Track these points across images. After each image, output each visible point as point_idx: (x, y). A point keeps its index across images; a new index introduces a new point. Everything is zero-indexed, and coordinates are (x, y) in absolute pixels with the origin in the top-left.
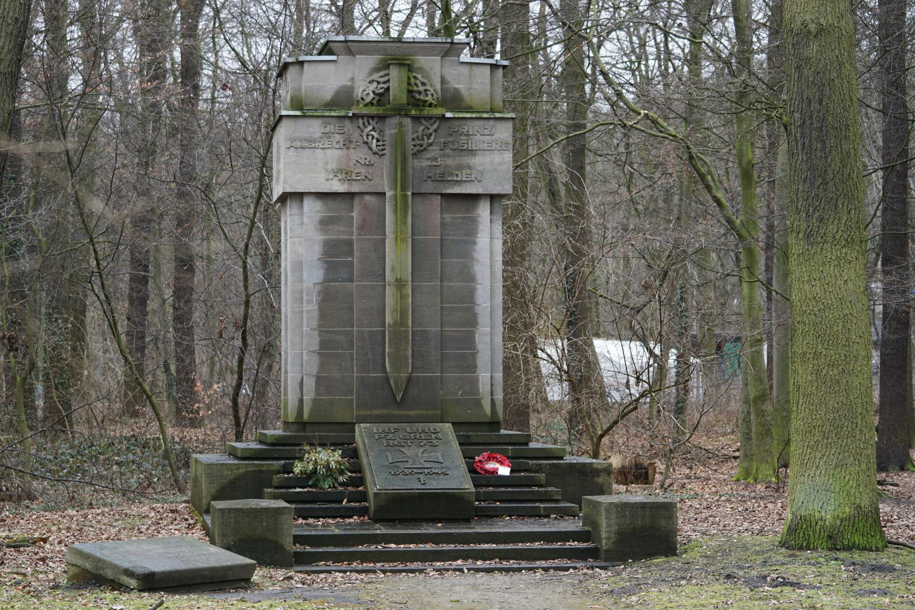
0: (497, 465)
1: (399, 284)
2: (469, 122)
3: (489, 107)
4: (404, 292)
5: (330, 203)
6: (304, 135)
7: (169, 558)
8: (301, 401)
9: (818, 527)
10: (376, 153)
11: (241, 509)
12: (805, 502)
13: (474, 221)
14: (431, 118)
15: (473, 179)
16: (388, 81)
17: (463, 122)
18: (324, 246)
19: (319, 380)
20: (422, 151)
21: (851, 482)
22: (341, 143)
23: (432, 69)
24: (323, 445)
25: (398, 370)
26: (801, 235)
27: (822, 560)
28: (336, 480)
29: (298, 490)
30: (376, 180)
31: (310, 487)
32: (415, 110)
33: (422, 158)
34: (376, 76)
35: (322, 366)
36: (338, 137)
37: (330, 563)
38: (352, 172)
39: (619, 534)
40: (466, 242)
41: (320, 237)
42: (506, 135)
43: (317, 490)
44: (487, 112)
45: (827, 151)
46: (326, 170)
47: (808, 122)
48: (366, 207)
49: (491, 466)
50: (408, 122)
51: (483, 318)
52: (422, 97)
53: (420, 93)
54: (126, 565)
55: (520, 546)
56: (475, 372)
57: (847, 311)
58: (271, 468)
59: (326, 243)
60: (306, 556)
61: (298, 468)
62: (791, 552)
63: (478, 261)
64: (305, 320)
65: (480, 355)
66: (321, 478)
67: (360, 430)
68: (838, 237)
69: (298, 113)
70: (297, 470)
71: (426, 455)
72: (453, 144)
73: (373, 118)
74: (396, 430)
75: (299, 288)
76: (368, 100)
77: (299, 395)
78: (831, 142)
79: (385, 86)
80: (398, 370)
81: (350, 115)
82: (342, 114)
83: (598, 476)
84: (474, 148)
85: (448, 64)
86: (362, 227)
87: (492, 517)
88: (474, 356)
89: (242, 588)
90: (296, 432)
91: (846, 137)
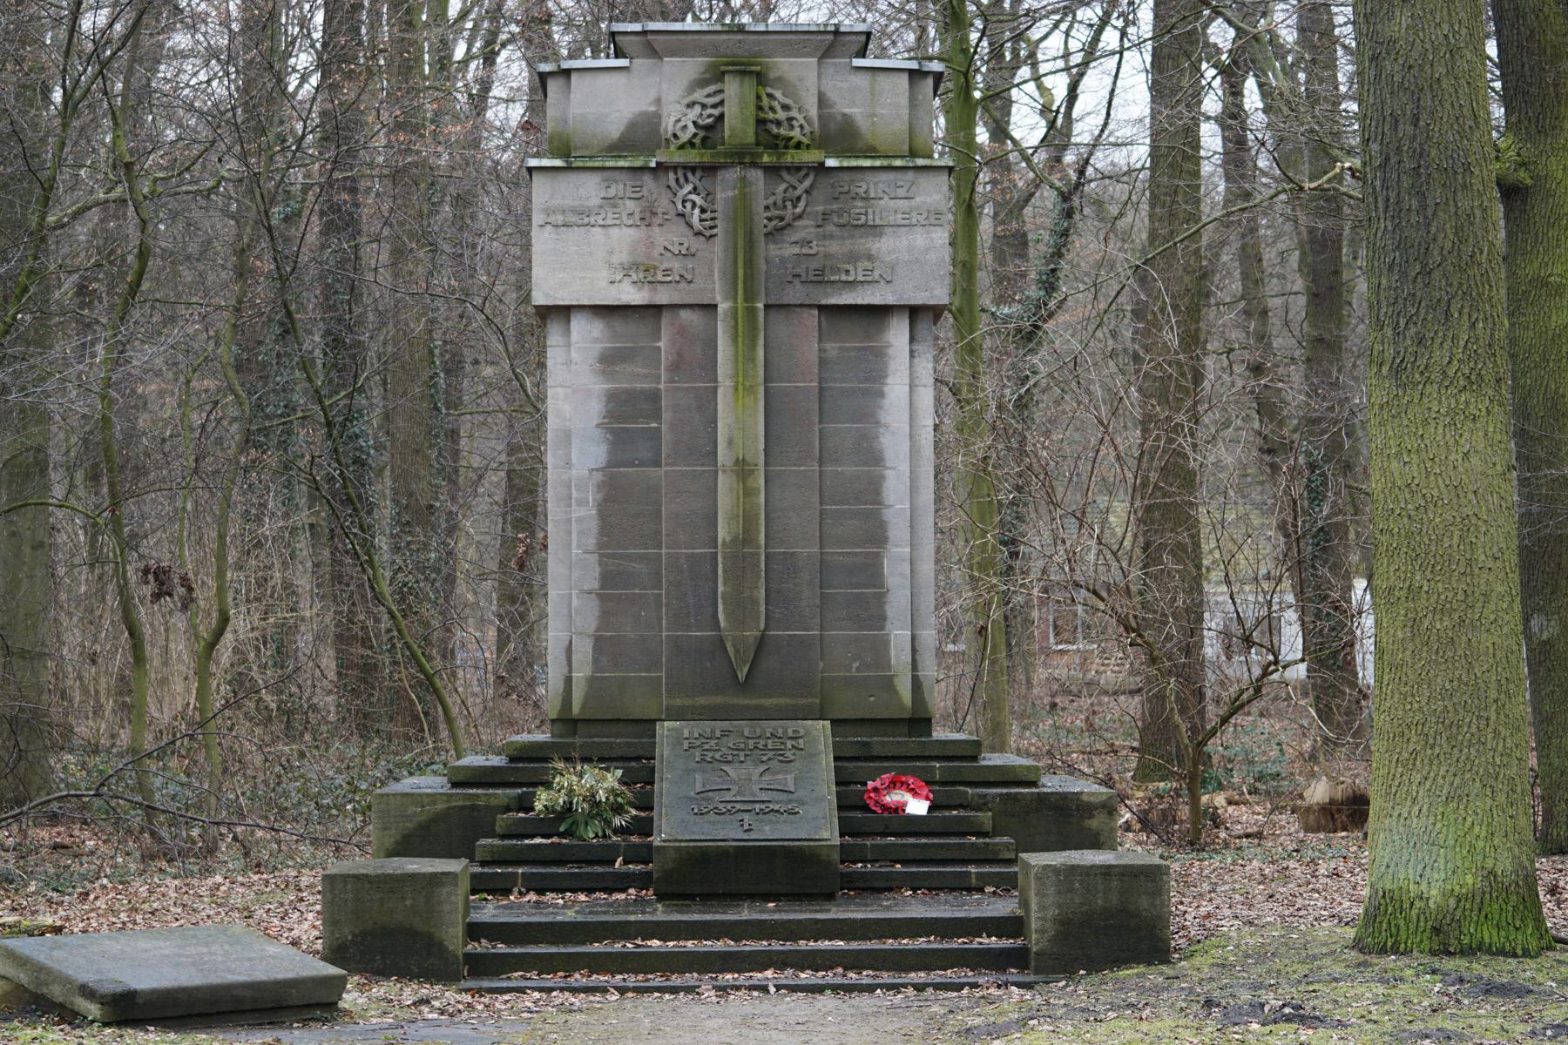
0: (908, 797)
1: (742, 469)
2: (869, 176)
3: (906, 147)
4: (750, 483)
5: (619, 324)
6: (570, 202)
7: (177, 964)
8: (568, 681)
9: (1414, 912)
10: (699, 234)
11: (366, 876)
12: (1392, 865)
13: (880, 354)
14: (799, 169)
15: (876, 277)
16: (722, 103)
17: (859, 175)
18: (608, 402)
19: (600, 643)
20: (783, 228)
21: (1477, 829)
22: (637, 217)
23: (801, 80)
24: (586, 760)
25: (750, 630)
26: (1385, 370)
27: (1409, 972)
28: (608, 823)
29: (538, 841)
30: (699, 283)
31: (561, 835)
32: (770, 155)
33: (783, 241)
34: (699, 95)
35: (605, 617)
36: (631, 205)
37: (533, 974)
38: (655, 268)
39: (1062, 923)
40: (865, 392)
41: (599, 386)
42: (937, 197)
43: (575, 842)
44: (902, 157)
45: (1430, 211)
46: (610, 265)
47: (1394, 160)
48: (682, 331)
49: (893, 797)
50: (757, 175)
51: (898, 530)
52: (783, 132)
53: (778, 123)
54: (86, 977)
55: (890, 944)
56: (883, 628)
57: (1468, 511)
58: (494, 802)
59: (612, 397)
60: (486, 964)
61: (542, 800)
62: (1362, 958)
63: (887, 426)
64: (574, 535)
65: (891, 597)
66: (581, 819)
67: (665, 729)
68: (1451, 373)
69: (558, 163)
70: (538, 806)
71: (766, 778)
72: (840, 216)
73: (693, 169)
74: (726, 733)
75: (565, 477)
76: (684, 137)
77: (566, 671)
78: (1436, 195)
79: (716, 112)
80: (750, 630)
81: (653, 165)
82: (638, 163)
83: (1091, 816)
84: (878, 222)
85: (831, 71)
86: (675, 367)
87: (881, 890)
88: (881, 598)
89: (316, 1020)
90: (561, 736)
91: (1464, 187)
